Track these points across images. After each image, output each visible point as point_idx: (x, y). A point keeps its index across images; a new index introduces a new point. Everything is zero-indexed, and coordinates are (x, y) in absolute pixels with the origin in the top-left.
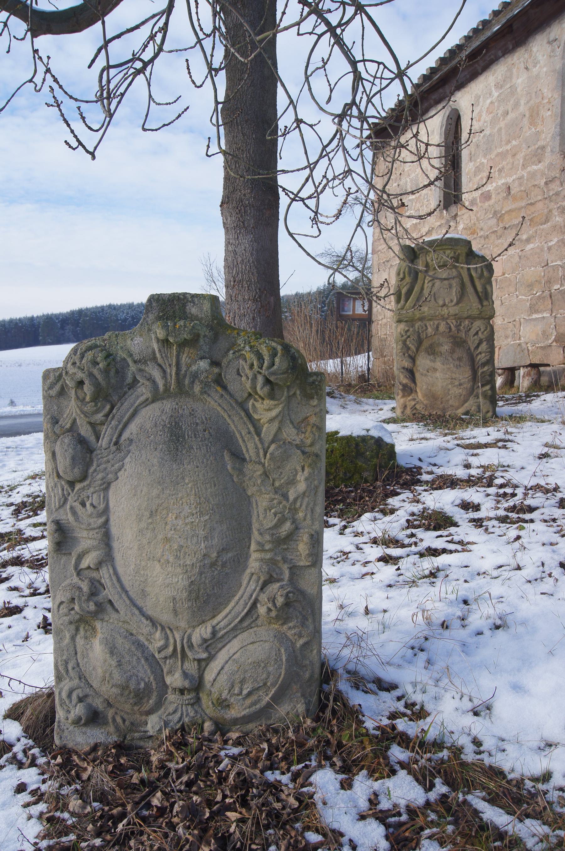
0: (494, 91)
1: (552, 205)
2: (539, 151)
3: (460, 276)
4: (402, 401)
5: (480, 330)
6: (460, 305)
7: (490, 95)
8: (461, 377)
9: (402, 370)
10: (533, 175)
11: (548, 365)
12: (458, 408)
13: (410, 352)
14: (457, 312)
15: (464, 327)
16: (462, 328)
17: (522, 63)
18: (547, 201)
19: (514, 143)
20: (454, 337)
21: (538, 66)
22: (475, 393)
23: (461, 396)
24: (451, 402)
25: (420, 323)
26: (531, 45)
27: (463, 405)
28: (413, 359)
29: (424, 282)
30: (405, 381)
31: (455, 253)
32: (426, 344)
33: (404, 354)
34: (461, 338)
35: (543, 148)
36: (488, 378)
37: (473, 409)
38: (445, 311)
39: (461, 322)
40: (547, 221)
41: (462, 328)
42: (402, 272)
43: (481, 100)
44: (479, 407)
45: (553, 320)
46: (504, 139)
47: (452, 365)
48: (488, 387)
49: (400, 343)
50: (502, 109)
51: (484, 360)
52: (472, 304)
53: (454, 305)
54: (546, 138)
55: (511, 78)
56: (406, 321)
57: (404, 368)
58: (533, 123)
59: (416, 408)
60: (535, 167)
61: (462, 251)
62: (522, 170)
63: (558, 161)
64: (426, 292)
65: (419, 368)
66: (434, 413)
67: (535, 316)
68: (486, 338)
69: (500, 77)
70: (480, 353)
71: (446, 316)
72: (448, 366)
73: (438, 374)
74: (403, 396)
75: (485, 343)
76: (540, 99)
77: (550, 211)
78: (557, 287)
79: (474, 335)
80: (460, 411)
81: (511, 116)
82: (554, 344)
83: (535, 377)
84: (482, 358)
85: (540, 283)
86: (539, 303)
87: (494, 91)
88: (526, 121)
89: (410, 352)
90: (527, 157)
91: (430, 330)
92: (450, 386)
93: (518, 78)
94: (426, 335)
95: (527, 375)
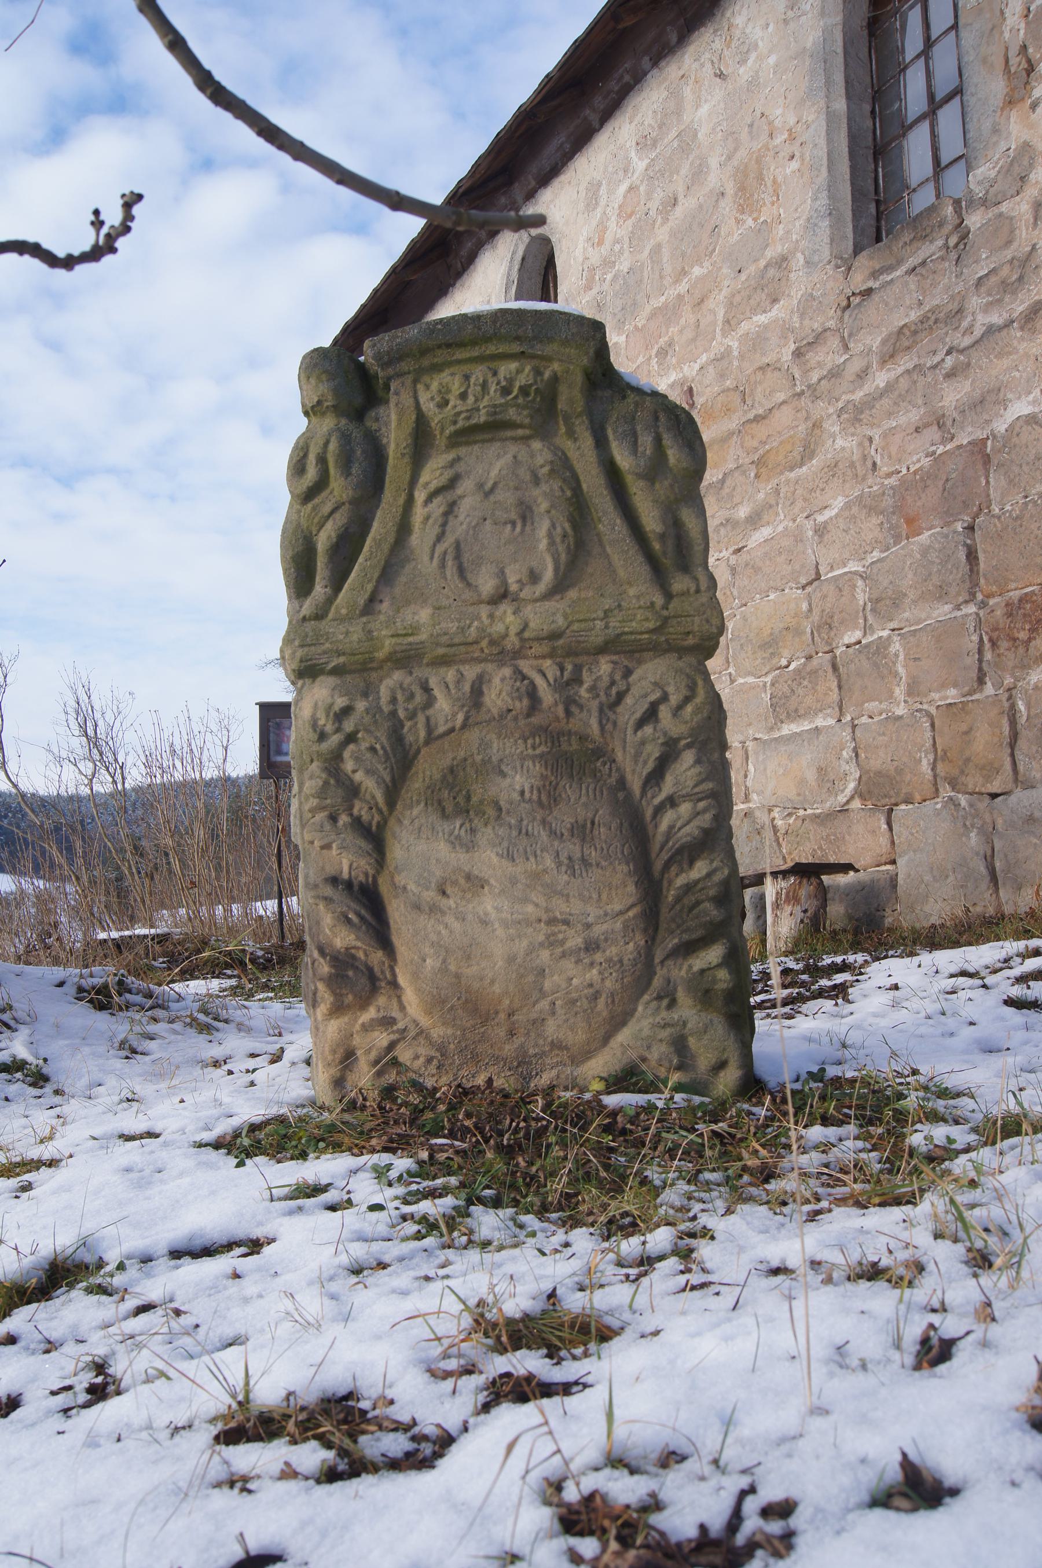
0: (635, 159)
1: (822, 409)
2: (772, 272)
3: (563, 468)
4: (333, 1028)
5: (665, 698)
6: (572, 594)
7: (626, 171)
8: (593, 913)
9: (328, 891)
10: (757, 342)
11: (846, 868)
12: (586, 1054)
13: (360, 808)
14: (561, 622)
15: (593, 689)
16: (583, 692)
17: (708, 65)
18: (804, 401)
19: (697, 271)
20: (553, 736)
21: (753, 56)
22: (657, 982)
23: (596, 996)
24: (552, 1029)
25: (398, 675)
26: (728, 14)
27: (606, 1040)
28: (375, 839)
29: (410, 501)
30: (343, 939)
31: (538, 372)
32: (428, 768)
33: (333, 818)
34: (583, 738)
35: (782, 262)
36: (712, 912)
37: (654, 1055)
38: (507, 620)
39: (578, 668)
40: (808, 453)
41: (583, 692)
42: (312, 458)
43: (603, 191)
44: (680, 1045)
45: (846, 735)
46: (668, 269)
47: (549, 862)
48: (714, 954)
49: (315, 767)
50: (659, 195)
51: (689, 832)
52: (625, 590)
53: (547, 596)
54: (788, 232)
55: (678, 112)
56: (337, 671)
57: (334, 881)
58: (746, 203)
59: (395, 1062)
60: (762, 319)
61: (568, 365)
62: (724, 335)
63: (830, 284)
64: (420, 539)
65: (400, 879)
66: (480, 1080)
67: (787, 729)
68: (694, 733)
69: (649, 120)
70: (672, 802)
71: (512, 642)
72: (532, 865)
73: (488, 904)
74: (338, 1009)
75: (688, 757)
76: (764, 137)
77: (817, 425)
78: (851, 637)
79: (640, 724)
80: (600, 1065)
81: (687, 205)
82: (856, 804)
83: (812, 905)
84: (681, 822)
85: (798, 632)
86: (800, 691)
87: (635, 159)
88: (727, 206)
89: (360, 808)
90: (737, 299)
91: (443, 704)
92: (545, 955)
93: (698, 107)
94: (430, 729)
95: (788, 900)
